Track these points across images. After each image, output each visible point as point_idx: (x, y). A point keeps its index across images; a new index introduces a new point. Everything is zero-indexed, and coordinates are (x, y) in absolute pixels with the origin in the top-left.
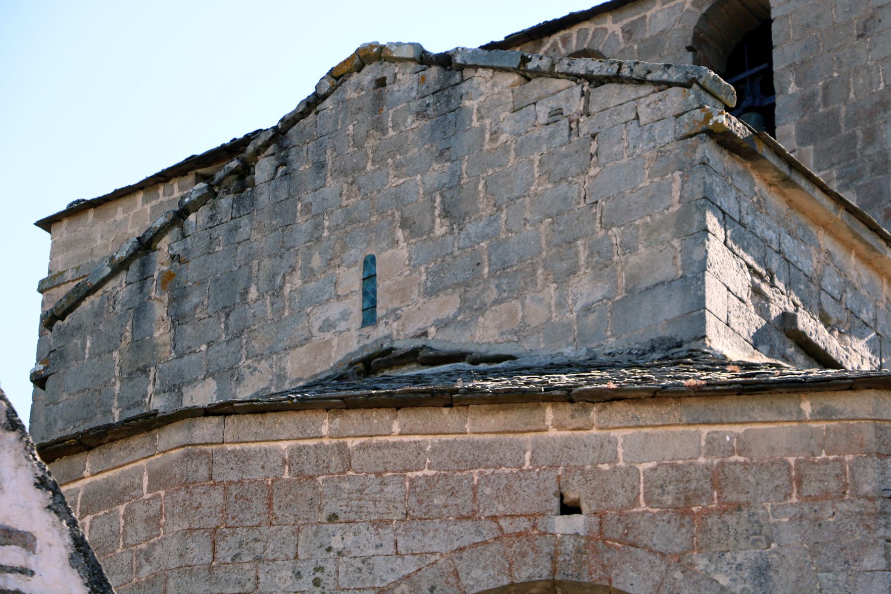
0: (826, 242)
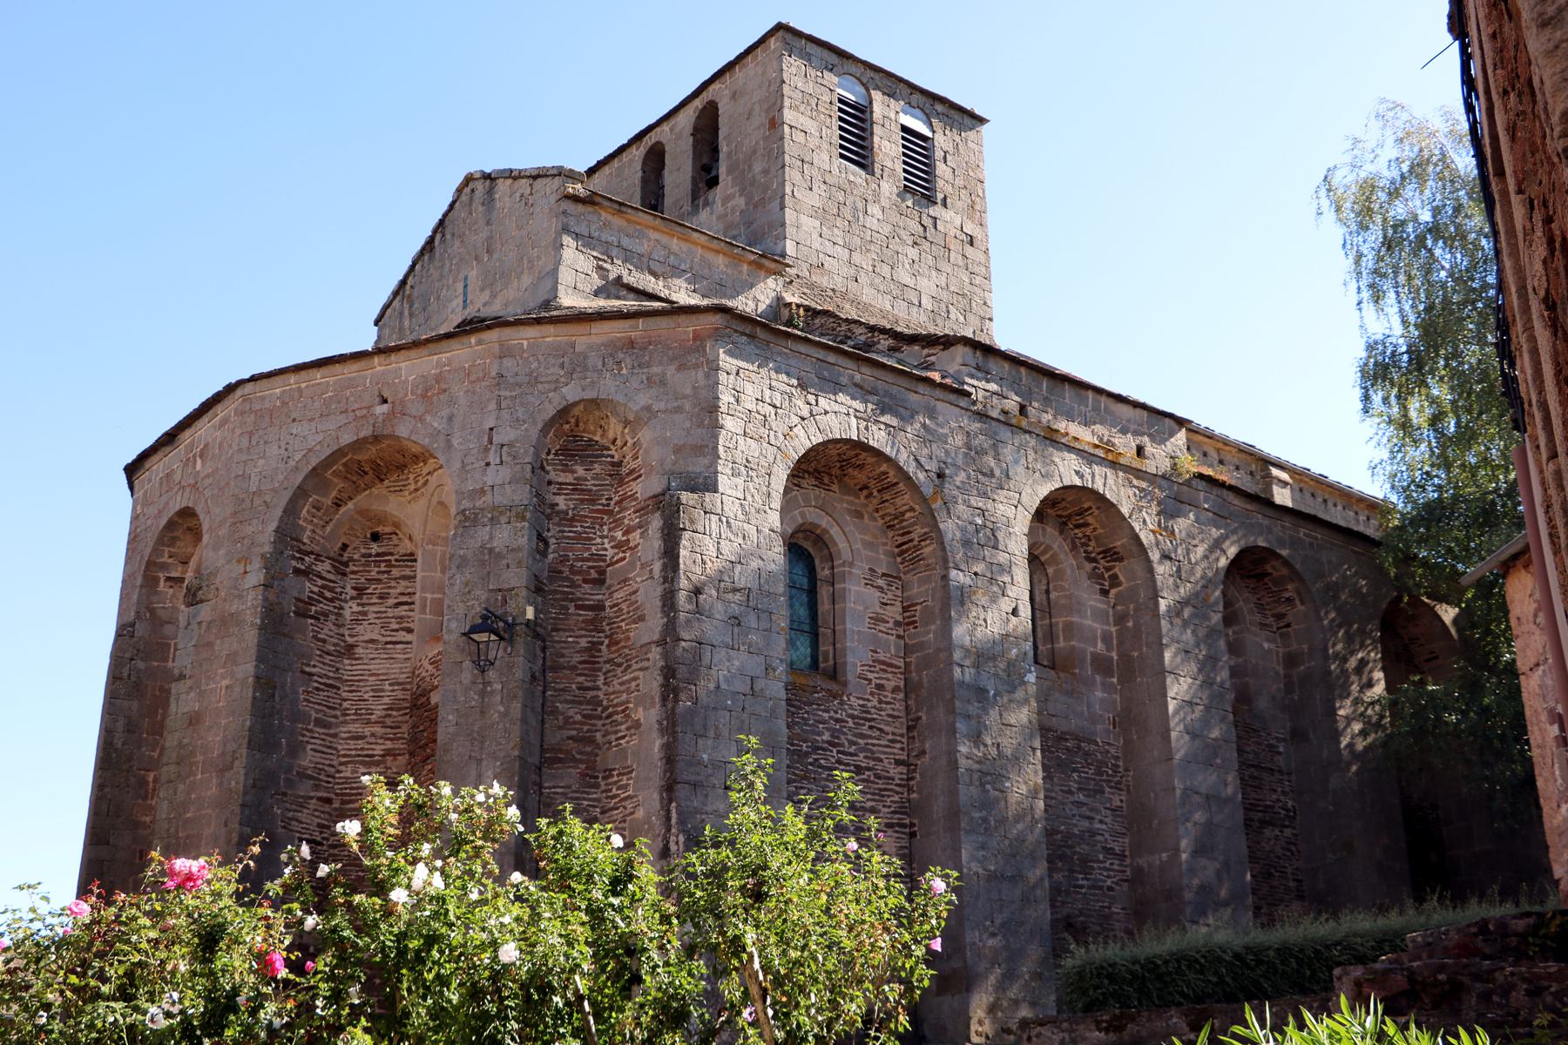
0: (654, 235)
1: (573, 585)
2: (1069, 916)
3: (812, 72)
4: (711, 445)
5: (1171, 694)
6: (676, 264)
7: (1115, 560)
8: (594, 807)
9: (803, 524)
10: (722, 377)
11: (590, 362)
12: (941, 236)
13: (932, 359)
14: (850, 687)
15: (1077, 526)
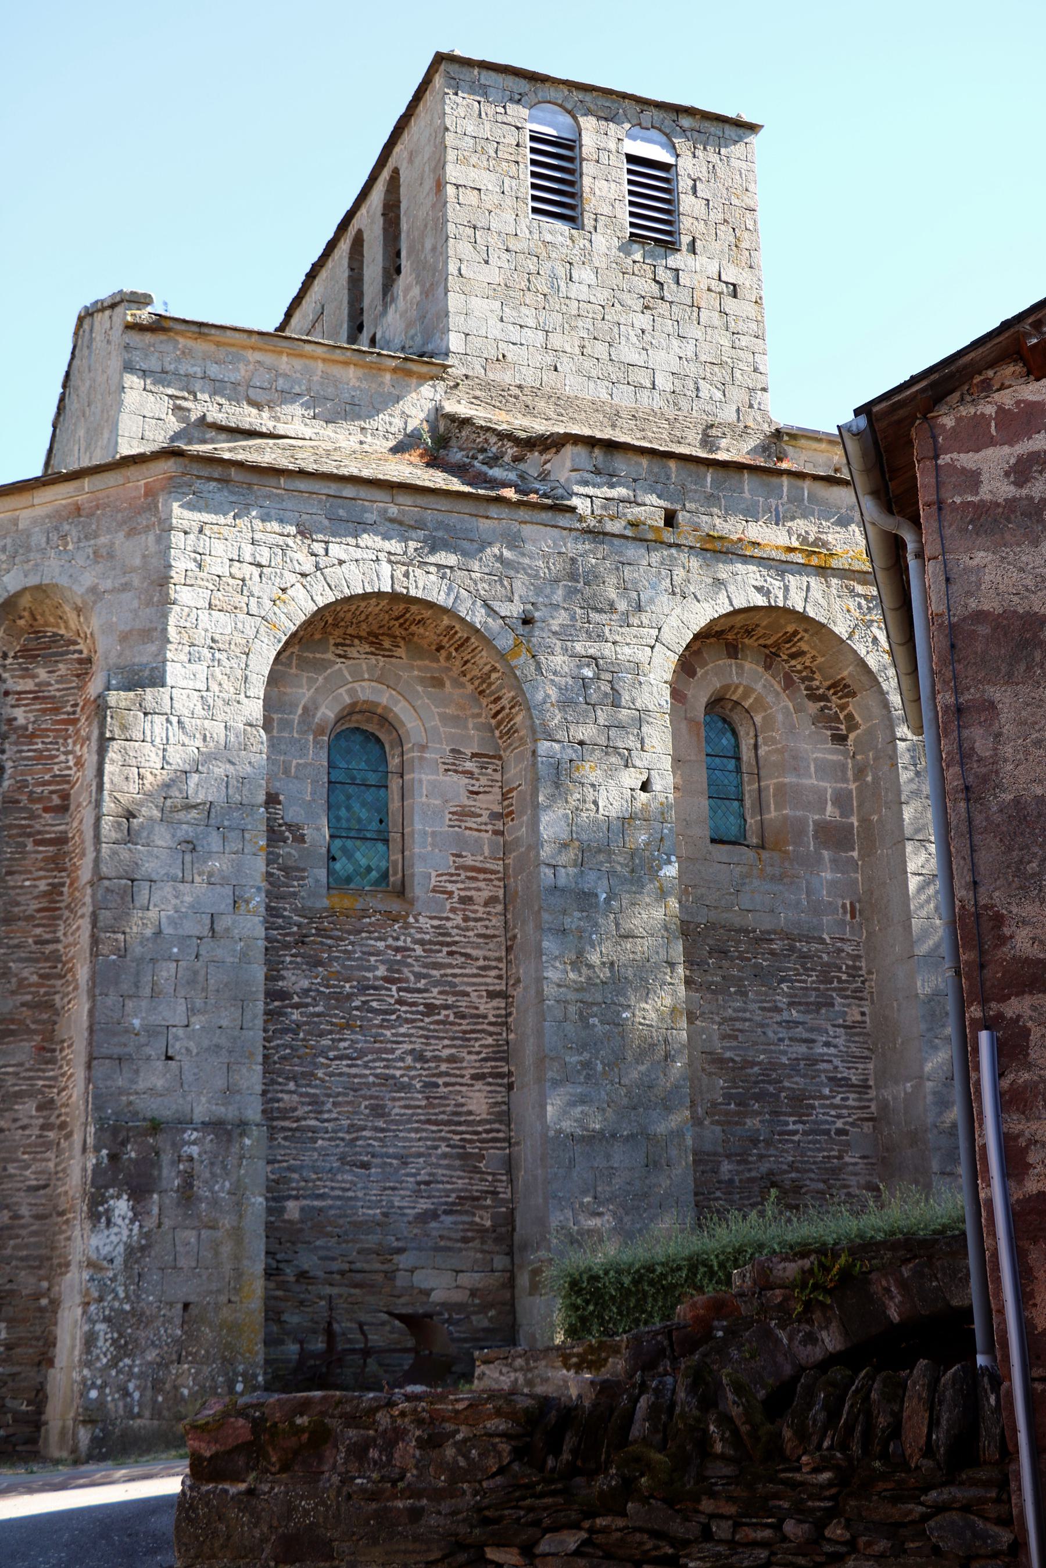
1: (33, 816)
2: (771, 1173)
3: (490, 109)
4: (160, 627)
5: (911, 867)
6: (286, 387)
7: (846, 696)
8: (50, 1087)
9: (354, 704)
10: (177, 539)
11: (34, 541)
12: (686, 292)
13: (548, 466)
14: (418, 906)
15: (793, 656)
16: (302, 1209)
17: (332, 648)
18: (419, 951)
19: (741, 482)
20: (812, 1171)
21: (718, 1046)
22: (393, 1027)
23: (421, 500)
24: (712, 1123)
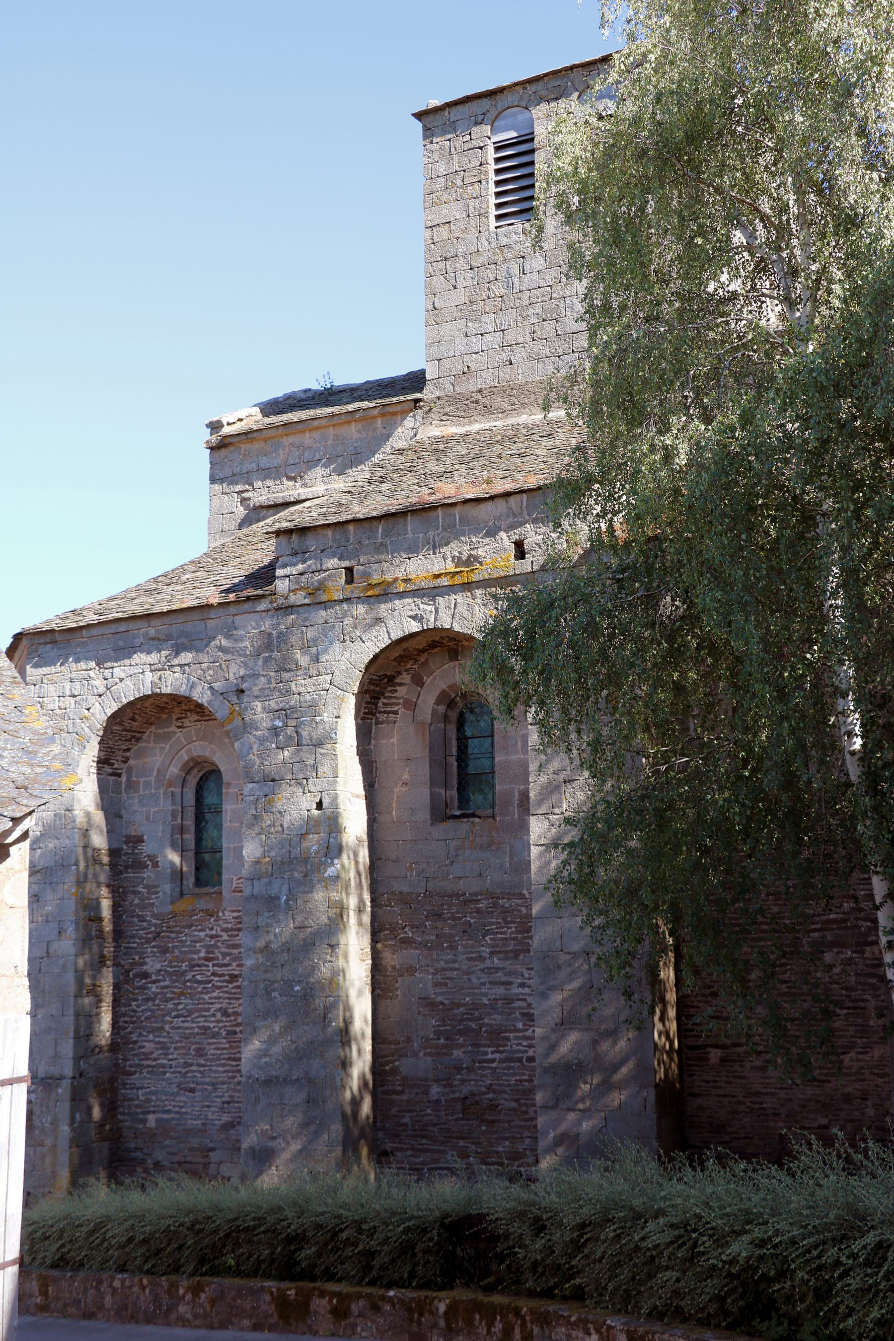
14: (225, 904)
16: (157, 1120)
17: (175, 722)
18: (225, 936)
19: (405, 525)
20: (505, 1092)
21: (431, 991)
22: (208, 993)
23: (166, 620)
24: (425, 1054)
